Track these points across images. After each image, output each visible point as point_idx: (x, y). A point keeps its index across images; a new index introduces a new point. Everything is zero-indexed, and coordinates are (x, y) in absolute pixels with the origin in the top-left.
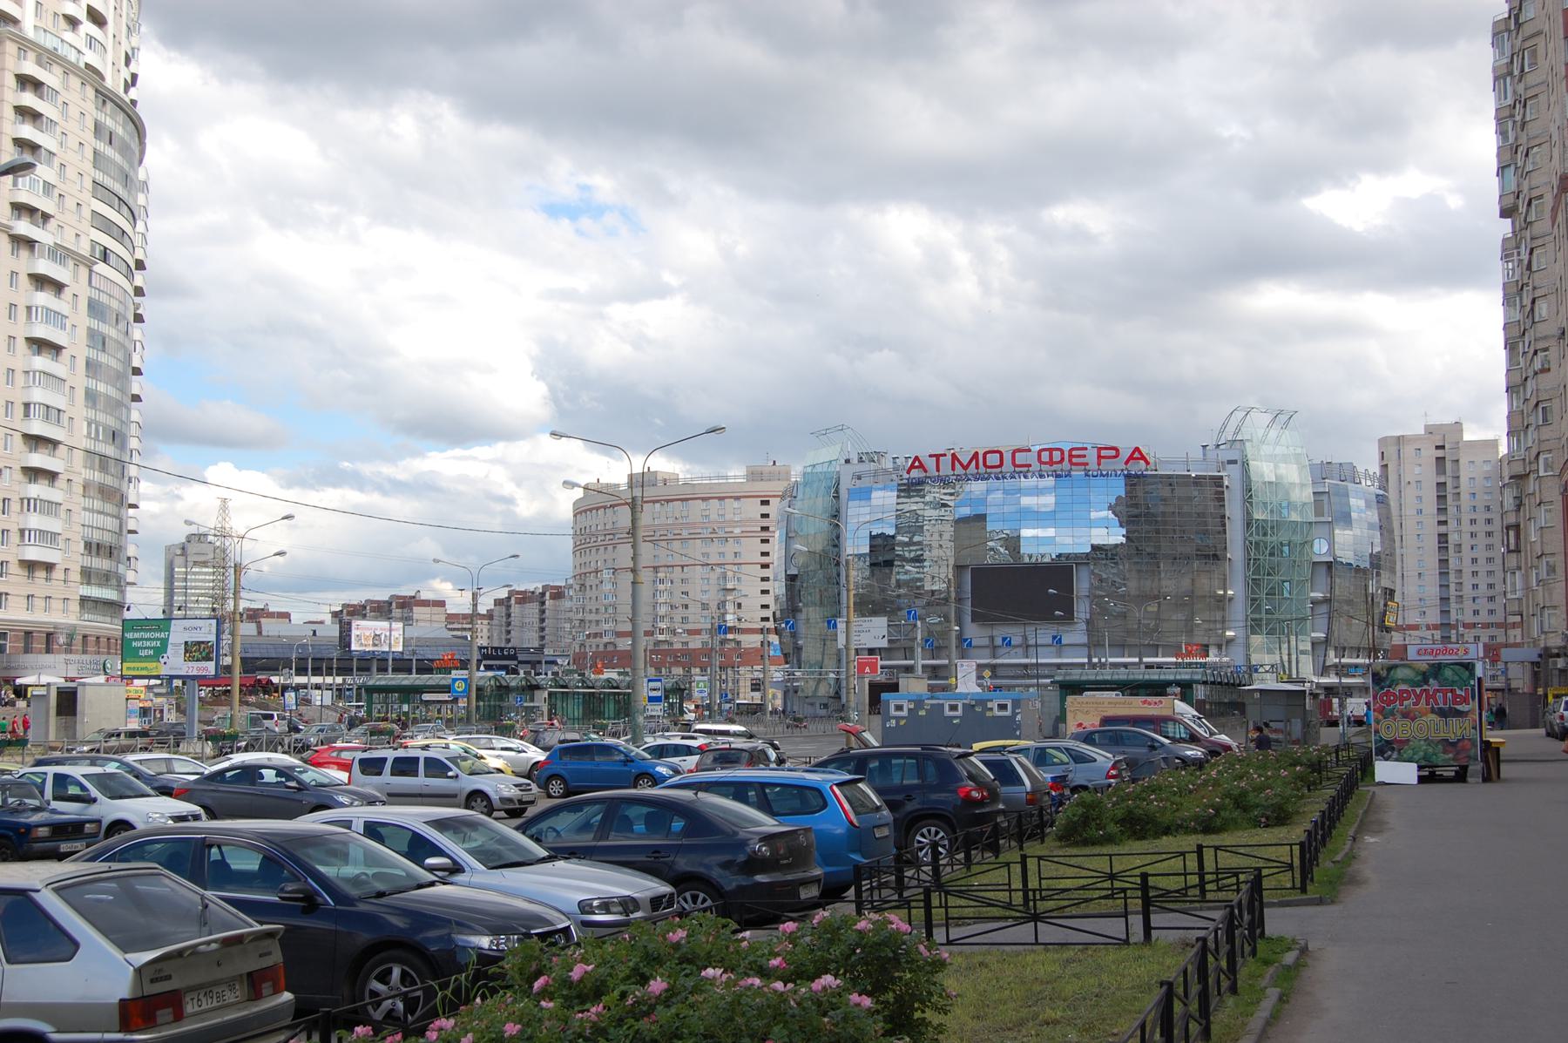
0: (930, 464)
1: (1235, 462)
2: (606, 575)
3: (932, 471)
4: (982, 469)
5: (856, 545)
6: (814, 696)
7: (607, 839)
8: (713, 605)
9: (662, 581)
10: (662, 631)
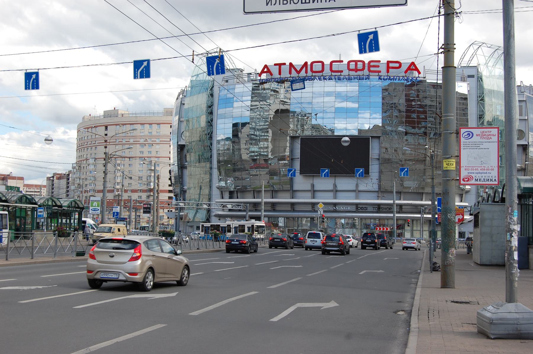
0: (275, 71)
1: (472, 76)
2: (91, 161)
3: (276, 75)
4: (310, 73)
5: (223, 131)
6: (193, 221)
7: (276, 198)
8: (144, 179)
9: (119, 165)
10: (118, 190)
